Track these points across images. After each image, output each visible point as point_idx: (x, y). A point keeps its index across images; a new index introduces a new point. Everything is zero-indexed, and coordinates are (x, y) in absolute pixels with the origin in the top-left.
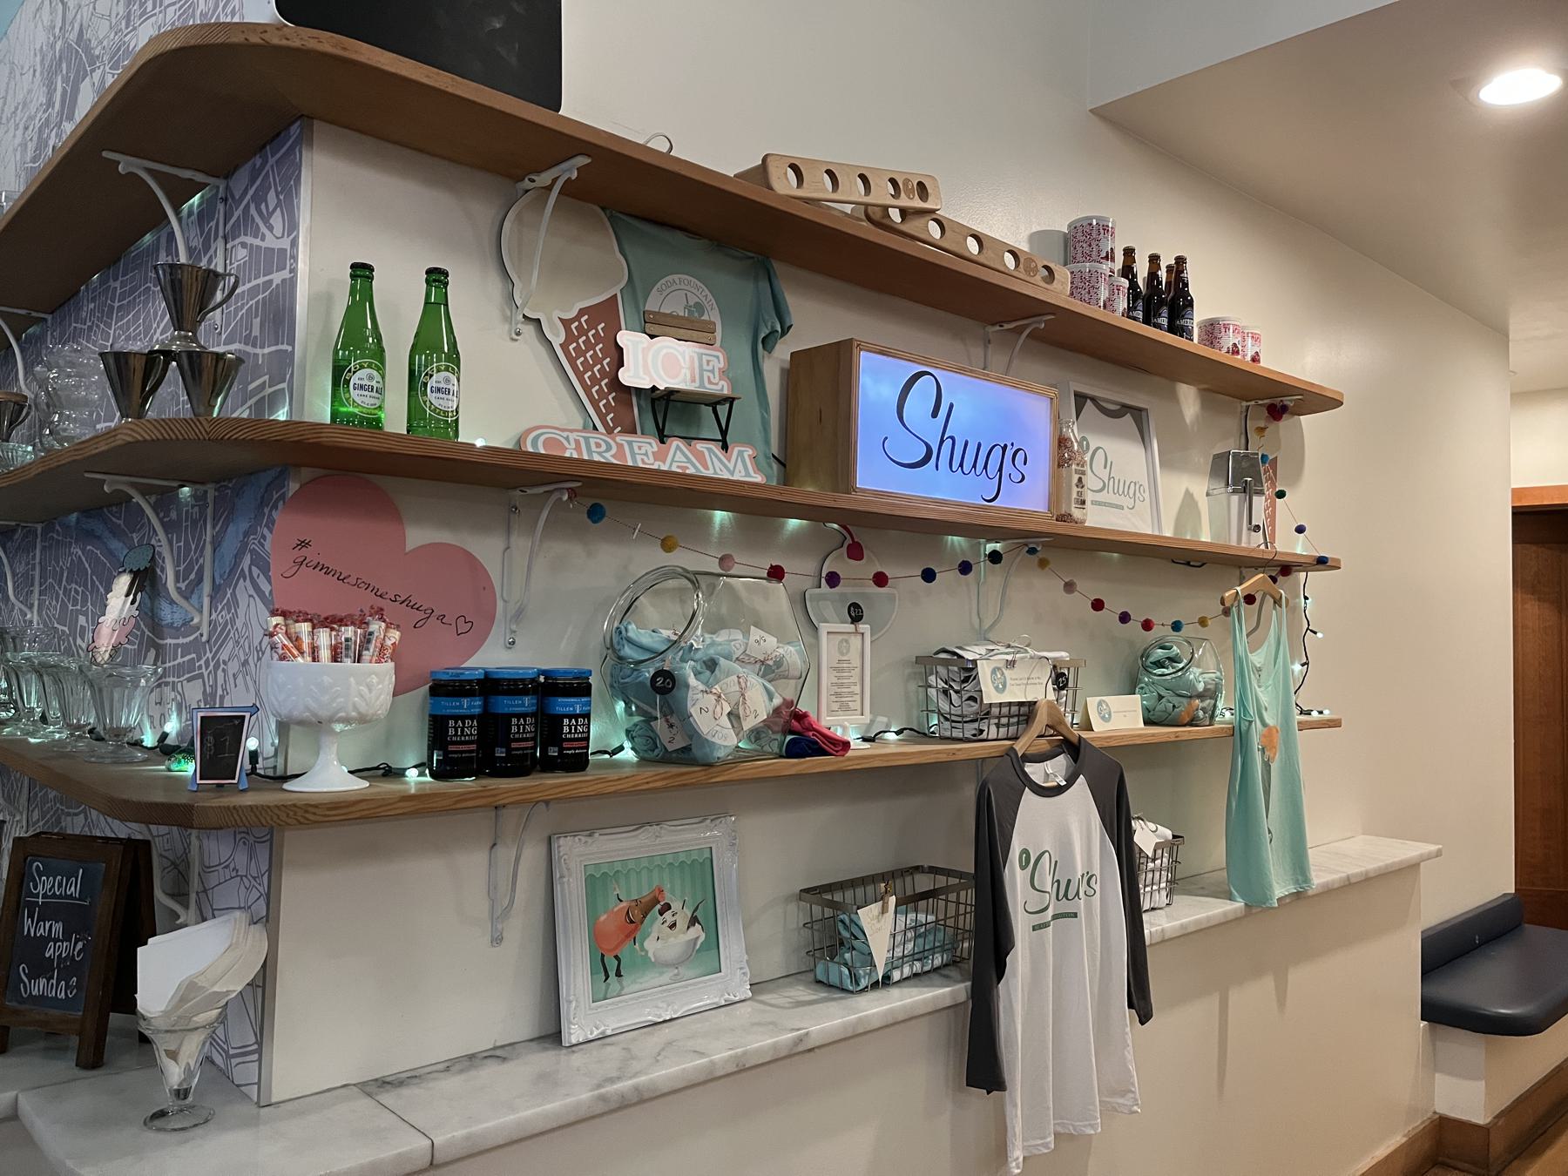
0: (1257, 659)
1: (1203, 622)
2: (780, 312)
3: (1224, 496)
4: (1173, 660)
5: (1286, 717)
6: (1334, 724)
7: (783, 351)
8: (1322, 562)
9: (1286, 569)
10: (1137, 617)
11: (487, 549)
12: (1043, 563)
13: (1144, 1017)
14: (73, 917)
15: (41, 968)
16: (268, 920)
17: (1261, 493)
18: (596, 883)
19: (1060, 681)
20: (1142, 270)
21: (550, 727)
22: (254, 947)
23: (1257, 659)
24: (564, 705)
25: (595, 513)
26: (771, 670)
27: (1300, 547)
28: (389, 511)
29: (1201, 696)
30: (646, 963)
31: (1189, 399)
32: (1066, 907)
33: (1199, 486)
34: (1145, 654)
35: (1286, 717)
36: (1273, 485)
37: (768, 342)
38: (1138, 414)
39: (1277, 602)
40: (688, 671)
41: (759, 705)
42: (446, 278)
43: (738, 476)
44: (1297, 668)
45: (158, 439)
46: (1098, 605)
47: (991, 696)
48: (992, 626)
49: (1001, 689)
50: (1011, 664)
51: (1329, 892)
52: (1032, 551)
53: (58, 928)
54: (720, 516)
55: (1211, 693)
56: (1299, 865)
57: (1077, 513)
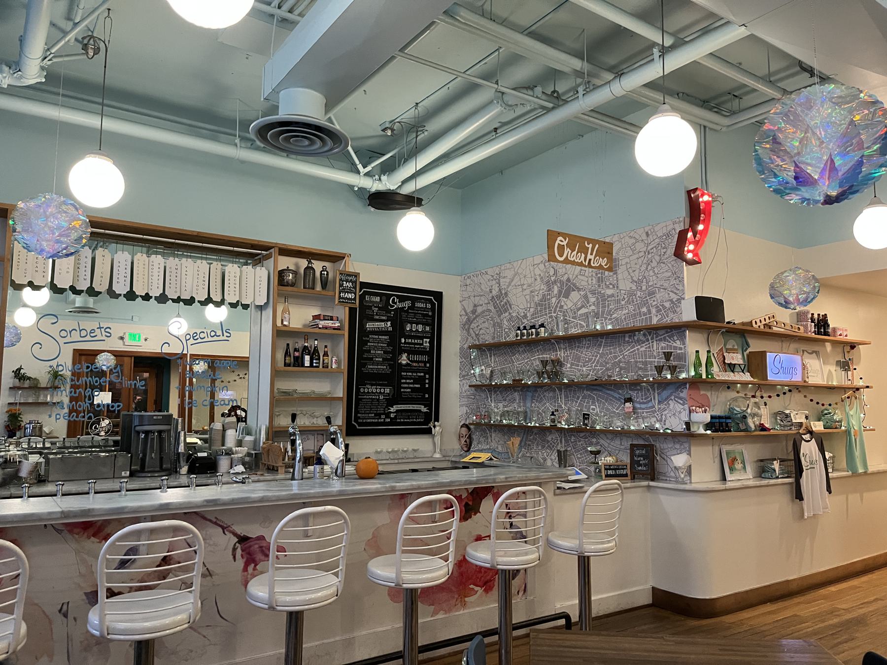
0: (851, 413)
1: (836, 404)
3: (840, 372)
4: (830, 413)
5: (860, 428)
6: (874, 430)
8: (867, 387)
9: (858, 389)
10: (821, 403)
11: (709, 394)
12: (799, 391)
13: (830, 493)
14: (645, 457)
15: (641, 465)
17: (850, 371)
18: (728, 453)
19: (807, 418)
20: (816, 316)
23: (851, 413)
25: (728, 388)
27: (861, 383)
28: (698, 389)
29: (838, 422)
31: (828, 346)
32: (812, 466)
33: (833, 368)
34: (822, 412)
35: (860, 428)
36: (852, 366)
38: (817, 353)
39: (856, 398)
43: (749, 379)
44: (862, 415)
46: (778, 395)
47: (794, 421)
48: (788, 405)
49: (796, 419)
50: (797, 414)
51: (873, 474)
52: (797, 389)
53: (642, 459)
55: (840, 421)
56: (865, 465)
57: (807, 380)
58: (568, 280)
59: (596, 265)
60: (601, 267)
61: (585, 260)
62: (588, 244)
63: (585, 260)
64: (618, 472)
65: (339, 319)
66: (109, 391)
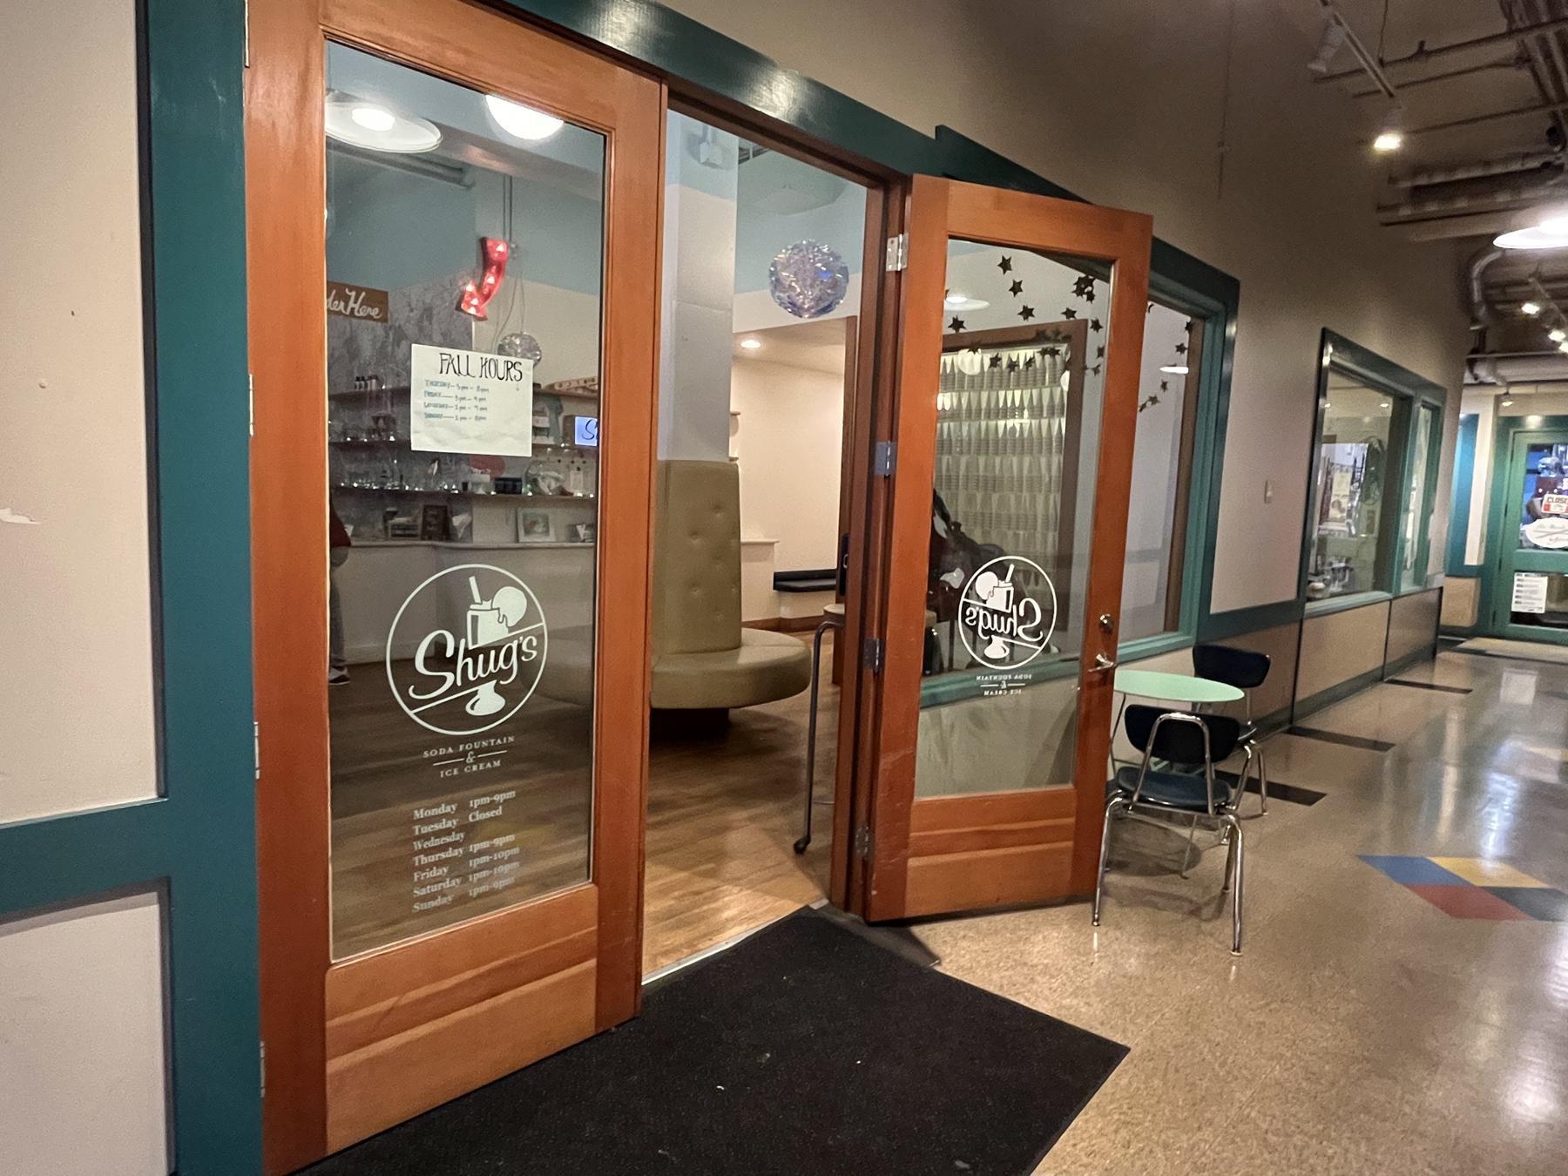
2: (561, 407)
7: (563, 415)
14: (436, 517)
15: (430, 526)
16: (471, 515)
18: (525, 517)
21: (515, 486)
22: (470, 518)
24: (518, 484)
26: (557, 480)
30: (535, 532)
37: (560, 413)
40: (539, 479)
41: (554, 485)
42: (542, 533)
45: (1533, 516)
54: (549, 449)
58: (400, 327)
59: (361, 314)
60: (369, 317)
61: (346, 308)
62: (350, 291)
63: (346, 308)
64: (407, 532)
65: (1085, 296)
66: (534, 446)
